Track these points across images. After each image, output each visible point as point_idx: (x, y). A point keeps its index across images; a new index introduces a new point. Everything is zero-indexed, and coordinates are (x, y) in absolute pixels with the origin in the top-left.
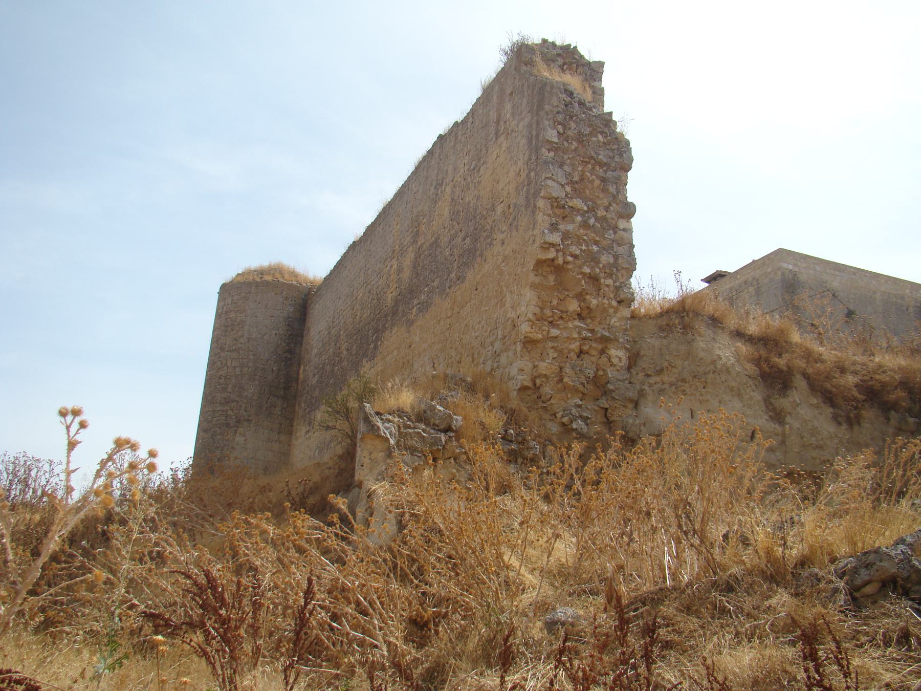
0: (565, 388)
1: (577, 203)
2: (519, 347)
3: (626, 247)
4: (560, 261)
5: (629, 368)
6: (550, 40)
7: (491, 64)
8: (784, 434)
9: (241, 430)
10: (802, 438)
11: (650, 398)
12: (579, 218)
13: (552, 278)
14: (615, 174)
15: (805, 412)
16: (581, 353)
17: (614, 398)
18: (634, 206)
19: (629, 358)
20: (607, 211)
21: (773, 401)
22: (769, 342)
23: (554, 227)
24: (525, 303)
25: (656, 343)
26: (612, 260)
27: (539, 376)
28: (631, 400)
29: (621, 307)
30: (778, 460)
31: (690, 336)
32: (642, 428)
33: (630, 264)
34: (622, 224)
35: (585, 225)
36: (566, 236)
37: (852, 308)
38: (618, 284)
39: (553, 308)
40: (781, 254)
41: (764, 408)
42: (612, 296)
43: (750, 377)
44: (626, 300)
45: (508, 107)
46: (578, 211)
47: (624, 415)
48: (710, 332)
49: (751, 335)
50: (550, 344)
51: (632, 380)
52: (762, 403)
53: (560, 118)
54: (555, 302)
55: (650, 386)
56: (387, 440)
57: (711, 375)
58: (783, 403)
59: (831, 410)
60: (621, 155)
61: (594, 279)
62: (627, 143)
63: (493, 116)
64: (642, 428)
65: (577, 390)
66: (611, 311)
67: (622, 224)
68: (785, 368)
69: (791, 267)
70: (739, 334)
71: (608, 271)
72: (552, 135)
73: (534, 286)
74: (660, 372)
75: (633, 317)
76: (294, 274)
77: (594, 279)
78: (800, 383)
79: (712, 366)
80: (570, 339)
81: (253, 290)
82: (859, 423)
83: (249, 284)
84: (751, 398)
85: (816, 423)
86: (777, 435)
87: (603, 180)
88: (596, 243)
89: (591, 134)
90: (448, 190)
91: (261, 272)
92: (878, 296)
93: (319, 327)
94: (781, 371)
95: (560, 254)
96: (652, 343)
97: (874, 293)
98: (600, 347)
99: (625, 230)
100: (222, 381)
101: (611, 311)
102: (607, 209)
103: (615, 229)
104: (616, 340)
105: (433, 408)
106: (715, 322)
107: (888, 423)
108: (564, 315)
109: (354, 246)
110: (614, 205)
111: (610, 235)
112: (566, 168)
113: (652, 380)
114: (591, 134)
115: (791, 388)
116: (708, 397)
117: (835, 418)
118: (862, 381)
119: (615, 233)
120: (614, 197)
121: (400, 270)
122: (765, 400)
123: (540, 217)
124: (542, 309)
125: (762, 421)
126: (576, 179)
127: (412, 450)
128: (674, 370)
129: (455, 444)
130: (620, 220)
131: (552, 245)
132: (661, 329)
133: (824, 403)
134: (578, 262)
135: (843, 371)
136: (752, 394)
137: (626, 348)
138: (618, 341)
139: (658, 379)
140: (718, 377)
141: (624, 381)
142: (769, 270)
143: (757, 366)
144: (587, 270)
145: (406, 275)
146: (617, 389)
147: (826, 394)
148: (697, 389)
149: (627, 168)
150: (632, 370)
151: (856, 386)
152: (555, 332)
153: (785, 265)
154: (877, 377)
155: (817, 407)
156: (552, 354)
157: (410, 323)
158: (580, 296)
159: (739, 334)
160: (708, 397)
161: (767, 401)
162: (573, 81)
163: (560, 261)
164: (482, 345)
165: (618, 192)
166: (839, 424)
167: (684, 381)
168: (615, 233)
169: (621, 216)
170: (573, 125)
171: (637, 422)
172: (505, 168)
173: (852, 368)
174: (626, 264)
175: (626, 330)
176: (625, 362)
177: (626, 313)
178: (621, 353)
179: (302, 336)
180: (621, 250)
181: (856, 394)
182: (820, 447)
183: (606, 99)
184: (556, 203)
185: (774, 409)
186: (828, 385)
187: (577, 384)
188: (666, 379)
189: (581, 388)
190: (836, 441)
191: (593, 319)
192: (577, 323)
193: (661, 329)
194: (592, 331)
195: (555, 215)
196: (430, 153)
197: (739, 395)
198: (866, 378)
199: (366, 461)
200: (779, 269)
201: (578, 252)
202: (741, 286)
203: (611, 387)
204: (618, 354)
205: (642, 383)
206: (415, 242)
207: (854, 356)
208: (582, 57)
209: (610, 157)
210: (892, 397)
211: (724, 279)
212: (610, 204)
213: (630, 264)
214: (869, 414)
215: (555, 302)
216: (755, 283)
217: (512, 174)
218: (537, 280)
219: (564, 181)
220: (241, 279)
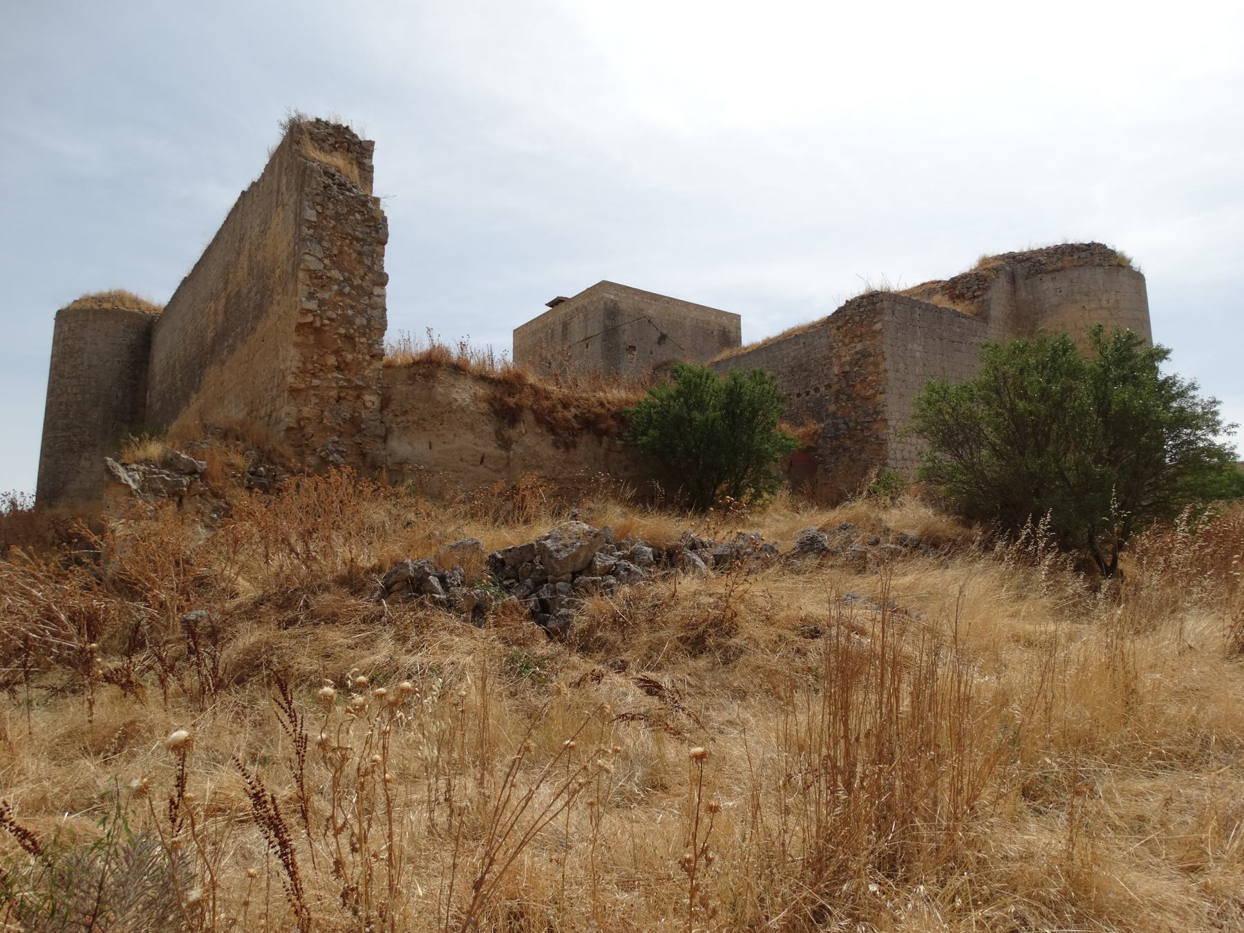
0: (325, 428)
1: (335, 274)
2: (286, 394)
4: (318, 324)
5: (381, 410)
6: (324, 119)
7: (274, 137)
8: (508, 457)
9: (86, 455)
11: (396, 434)
12: (336, 287)
13: (312, 338)
14: (371, 248)
16: (339, 399)
23: (311, 296)
24: (291, 358)
25: (404, 389)
26: (365, 322)
27: (303, 418)
28: (379, 436)
34: (377, 291)
35: (340, 293)
36: (322, 303)
37: (665, 332)
39: (313, 362)
40: (604, 285)
44: (379, 355)
45: (284, 181)
46: (336, 281)
47: (375, 450)
50: (313, 392)
53: (318, 199)
54: (315, 358)
56: (128, 486)
58: (512, 433)
60: (377, 232)
61: (349, 338)
62: (385, 220)
63: (275, 186)
65: (334, 430)
66: (365, 364)
67: (377, 291)
72: (311, 215)
73: (296, 344)
74: (405, 413)
75: (389, 366)
76: (136, 301)
77: (349, 338)
78: (529, 417)
80: (329, 388)
81: (91, 317)
82: (575, 447)
83: (86, 312)
85: (538, 448)
87: (360, 253)
88: (352, 307)
89: (349, 213)
90: (247, 246)
91: (100, 299)
93: (161, 356)
94: (510, 408)
95: (318, 318)
96: (401, 389)
98: (355, 394)
99: (379, 296)
100: (63, 407)
101: (365, 364)
102: (362, 278)
103: (370, 295)
104: (370, 387)
105: (178, 457)
108: (324, 368)
109: (185, 281)
111: (365, 300)
112: (325, 244)
113: (399, 420)
114: (349, 213)
117: (555, 445)
121: (216, 313)
123: (300, 286)
124: (304, 363)
125: (491, 449)
126: (335, 252)
127: (156, 492)
129: (200, 483)
131: (310, 311)
134: (334, 324)
135: (566, 406)
139: (404, 418)
144: (342, 331)
145: (220, 318)
147: (547, 421)
149: (383, 242)
151: (576, 416)
152: (316, 382)
153: (607, 296)
156: (314, 400)
157: (223, 363)
158: (337, 352)
161: (498, 433)
162: (337, 161)
163: (318, 324)
164: (266, 390)
165: (373, 263)
166: (558, 448)
169: (376, 284)
170: (331, 206)
171: (383, 453)
172: (279, 240)
173: (575, 403)
174: (379, 325)
178: (374, 398)
179: (148, 363)
183: (375, 175)
184: (313, 274)
187: (334, 425)
188: (410, 418)
189: (338, 428)
191: (350, 370)
192: (336, 374)
193: (410, 378)
194: (349, 381)
195: (314, 285)
196: (237, 205)
197: (473, 429)
199: (112, 504)
201: (334, 316)
203: (363, 426)
204: (371, 399)
205: (392, 422)
206: (226, 289)
208: (354, 136)
210: (603, 426)
215: (315, 358)
217: (285, 243)
218: (299, 339)
219: (321, 255)
220: (78, 306)
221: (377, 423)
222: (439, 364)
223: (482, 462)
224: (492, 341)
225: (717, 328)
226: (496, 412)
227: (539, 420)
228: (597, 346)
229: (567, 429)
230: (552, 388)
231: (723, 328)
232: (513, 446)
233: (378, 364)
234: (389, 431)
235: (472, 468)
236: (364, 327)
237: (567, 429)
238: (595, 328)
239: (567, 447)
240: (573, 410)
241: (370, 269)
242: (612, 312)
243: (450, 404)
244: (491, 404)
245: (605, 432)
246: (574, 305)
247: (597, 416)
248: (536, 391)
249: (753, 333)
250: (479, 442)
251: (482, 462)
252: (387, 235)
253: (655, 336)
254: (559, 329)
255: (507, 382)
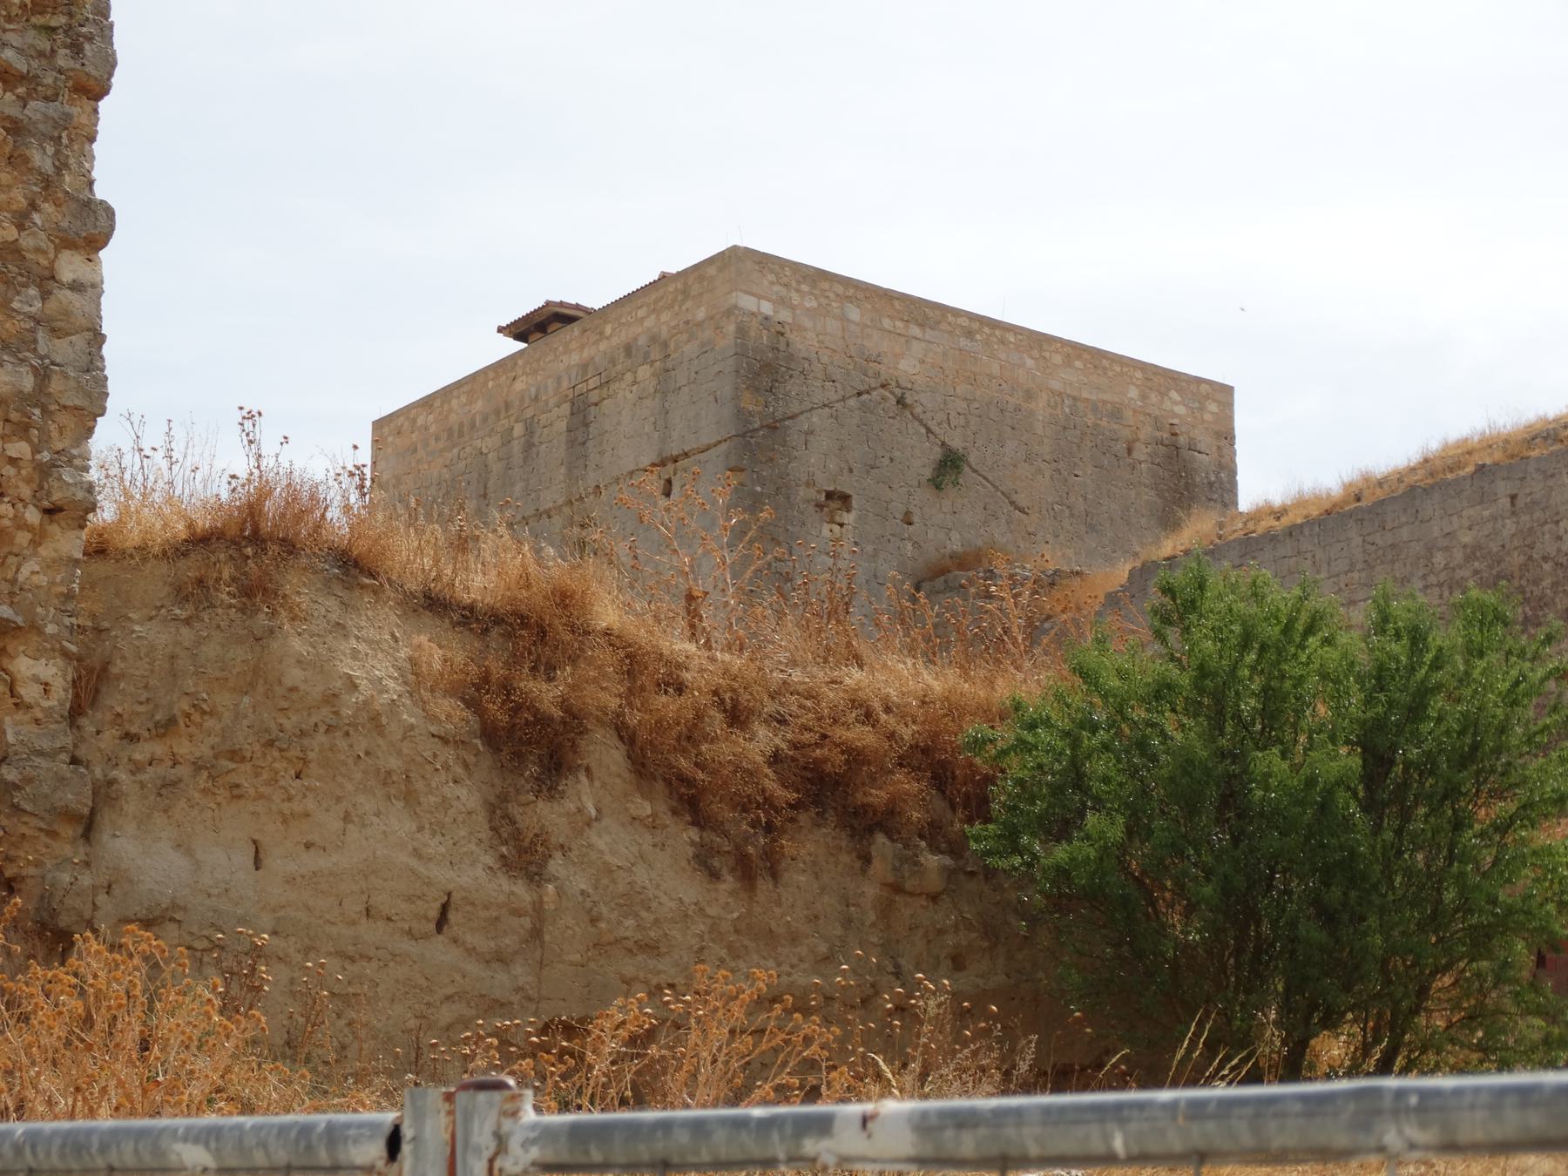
3: (79, 340)
5: (75, 713)
8: (538, 907)
10: (593, 921)
11: (131, 806)
14: (53, 109)
15: (613, 842)
17: (17, 809)
18: (110, 213)
19: (75, 683)
20: (20, 227)
21: (515, 810)
22: (530, 630)
26: (28, 383)
28: (69, 816)
29: (54, 529)
30: (518, 989)
31: (262, 620)
32: (102, 898)
33: (89, 395)
34: (70, 267)
37: (956, 443)
38: (45, 456)
40: (738, 264)
41: (485, 834)
42: (26, 492)
43: (444, 740)
44: (70, 510)
48: (332, 603)
49: (471, 608)
51: (82, 752)
52: (481, 818)
55: (136, 768)
57: (321, 738)
58: (548, 816)
59: (694, 834)
60: (76, 49)
64: (102, 898)
66: (23, 538)
67: (70, 267)
68: (557, 713)
69: (767, 308)
70: (434, 604)
71: (14, 416)
74: (166, 728)
75: (99, 550)
79: (325, 711)
82: (775, 875)
84: (445, 803)
85: (641, 875)
86: (517, 913)
92: (1040, 407)
94: (542, 720)
96: (147, 636)
97: (1029, 396)
99: (77, 287)
101: (23, 538)
103: (47, 281)
104: (35, 628)
106: (353, 567)
107: (864, 871)
110: (48, 207)
113: (141, 753)
115: (573, 770)
116: (310, 804)
117: (705, 862)
118: (795, 746)
119: (45, 295)
120: (47, 183)
122: (491, 809)
125: (474, 873)
128: (210, 723)
130: (66, 255)
132: (181, 594)
133: (675, 812)
135: (737, 717)
136: (450, 790)
137: (66, 654)
138: (40, 631)
139: (159, 749)
140: (342, 744)
141: (50, 755)
142: (701, 314)
143: (470, 703)
146: (30, 781)
148: (273, 781)
149: (94, 89)
150: (83, 721)
151: (775, 759)
153: (748, 303)
154: (839, 733)
155: (653, 826)
159: (434, 604)
160: (310, 804)
161: (498, 814)
165: (61, 166)
166: (714, 875)
167: (235, 755)
168: (45, 295)
171: (86, 880)
173: (770, 707)
174: (69, 390)
175: (69, 596)
176: (61, 694)
177: (70, 543)
180: (64, 350)
181: (771, 784)
182: (650, 948)
185: (517, 835)
186: (684, 764)
188: (183, 748)
190: (701, 927)
193: (181, 594)
197: (410, 798)
198: (807, 737)
200: (729, 312)
202: (613, 362)
205: (111, 761)
207: (787, 659)
209: (41, 54)
210: (878, 796)
211: (575, 329)
212: (33, 206)
213: (89, 395)
214: (812, 846)
216: (656, 354)
221: (62, 766)
222: (290, 547)
223: (442, 922)
224: (323, 448)
225: (1146, 432)
226: (490, 735)
227: (644, 763)
228: (710, 489)
229: (744, 806)
230: (679, 645)
231: (1168, 438)
232: (556, 865)
233: (70, 543)
234: (105, 794)
235: (406, 945)
236: (25, 399)
237: (744, 806)
238: (703, 420)
239: (746, 872)
240: (762, 732)
241: (48, 184)
242: (766, 367)
243: (331, 698)
244: (472, 704)
245: (885, 821)
246: (615, 337)
247: (856, 757)
248: (633, 662)
249: (1283, 460)
250: (435, 846)
251: (442, 922)
252: (109, 63)
253: (923, 460)
254: (558, 420)
255: (524, 621)
